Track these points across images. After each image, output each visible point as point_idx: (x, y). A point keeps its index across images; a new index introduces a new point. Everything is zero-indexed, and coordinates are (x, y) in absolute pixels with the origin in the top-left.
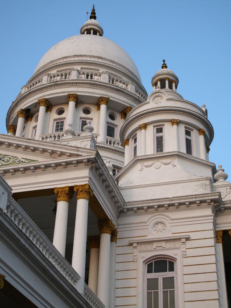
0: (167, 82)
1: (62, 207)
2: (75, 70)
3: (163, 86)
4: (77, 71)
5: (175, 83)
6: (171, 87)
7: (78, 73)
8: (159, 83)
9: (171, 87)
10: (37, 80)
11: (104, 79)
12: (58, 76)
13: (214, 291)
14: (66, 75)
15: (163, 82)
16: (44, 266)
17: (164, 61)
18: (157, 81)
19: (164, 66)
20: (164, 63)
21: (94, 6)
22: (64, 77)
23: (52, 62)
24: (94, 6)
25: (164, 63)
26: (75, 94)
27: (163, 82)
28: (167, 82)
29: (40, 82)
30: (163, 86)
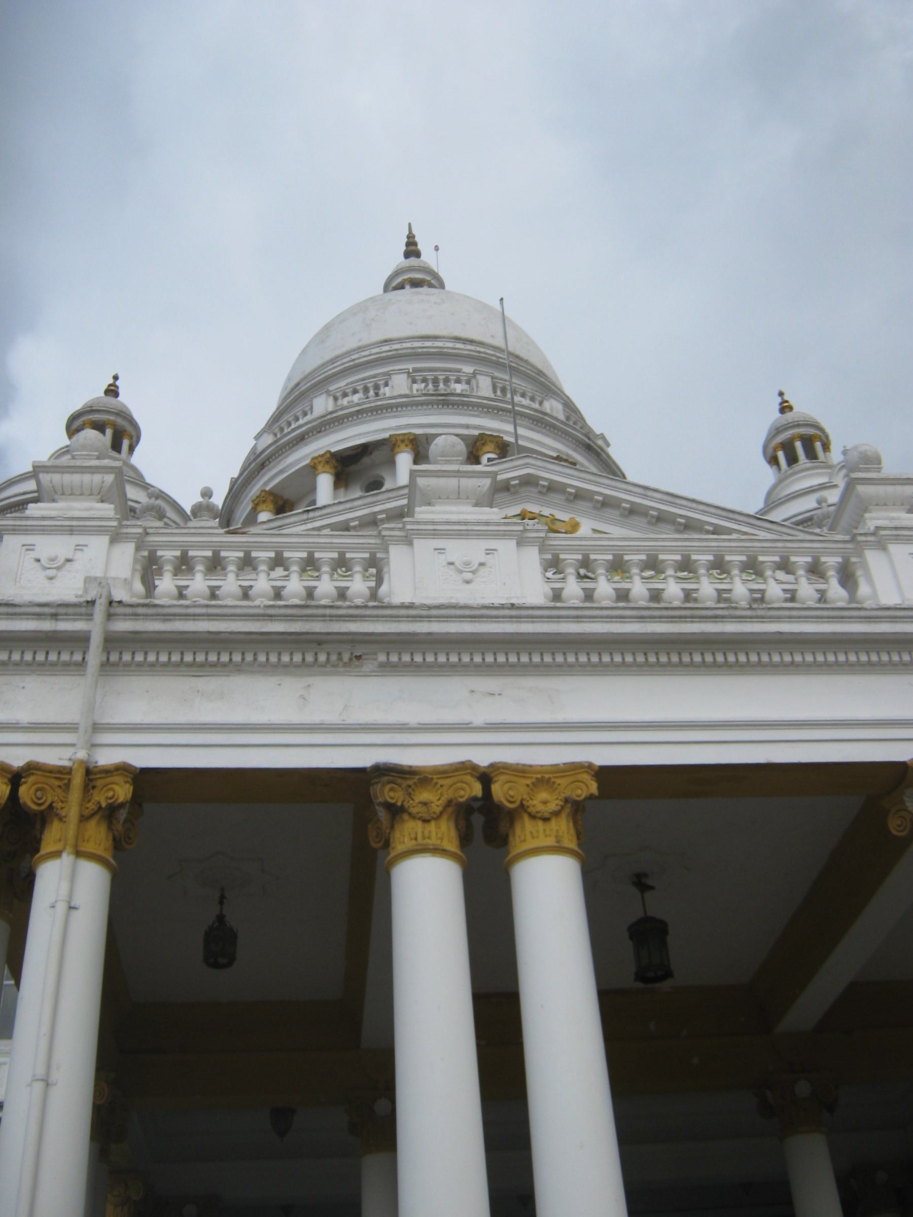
0: (798, 444)
1: (426, 896)
2: (400, 371)
3: (792, 460)
4: (405, 376)
5: (821, 440)
6: (811, 454)
7: (410, 380)
8: (781, 455)
9: (811, 454)
10: (297, 410)
11: (484, 386)
12: (355, 392)
13: (647, 746)
14: (377, 387)
15: (788, 447)
16: (55, 632)
17: (781, 394)
18: (775, 450)
19: (785, 408)
20: (782, 399)
21: (410, 225)
22: (372, 393)
23: (333, 361)
24: (410, 225)
25: (782, 399)
26: (410, 433)
27: (788, 447)
28: (798, 444)
29: (305, 414)
30: (792, 460)
